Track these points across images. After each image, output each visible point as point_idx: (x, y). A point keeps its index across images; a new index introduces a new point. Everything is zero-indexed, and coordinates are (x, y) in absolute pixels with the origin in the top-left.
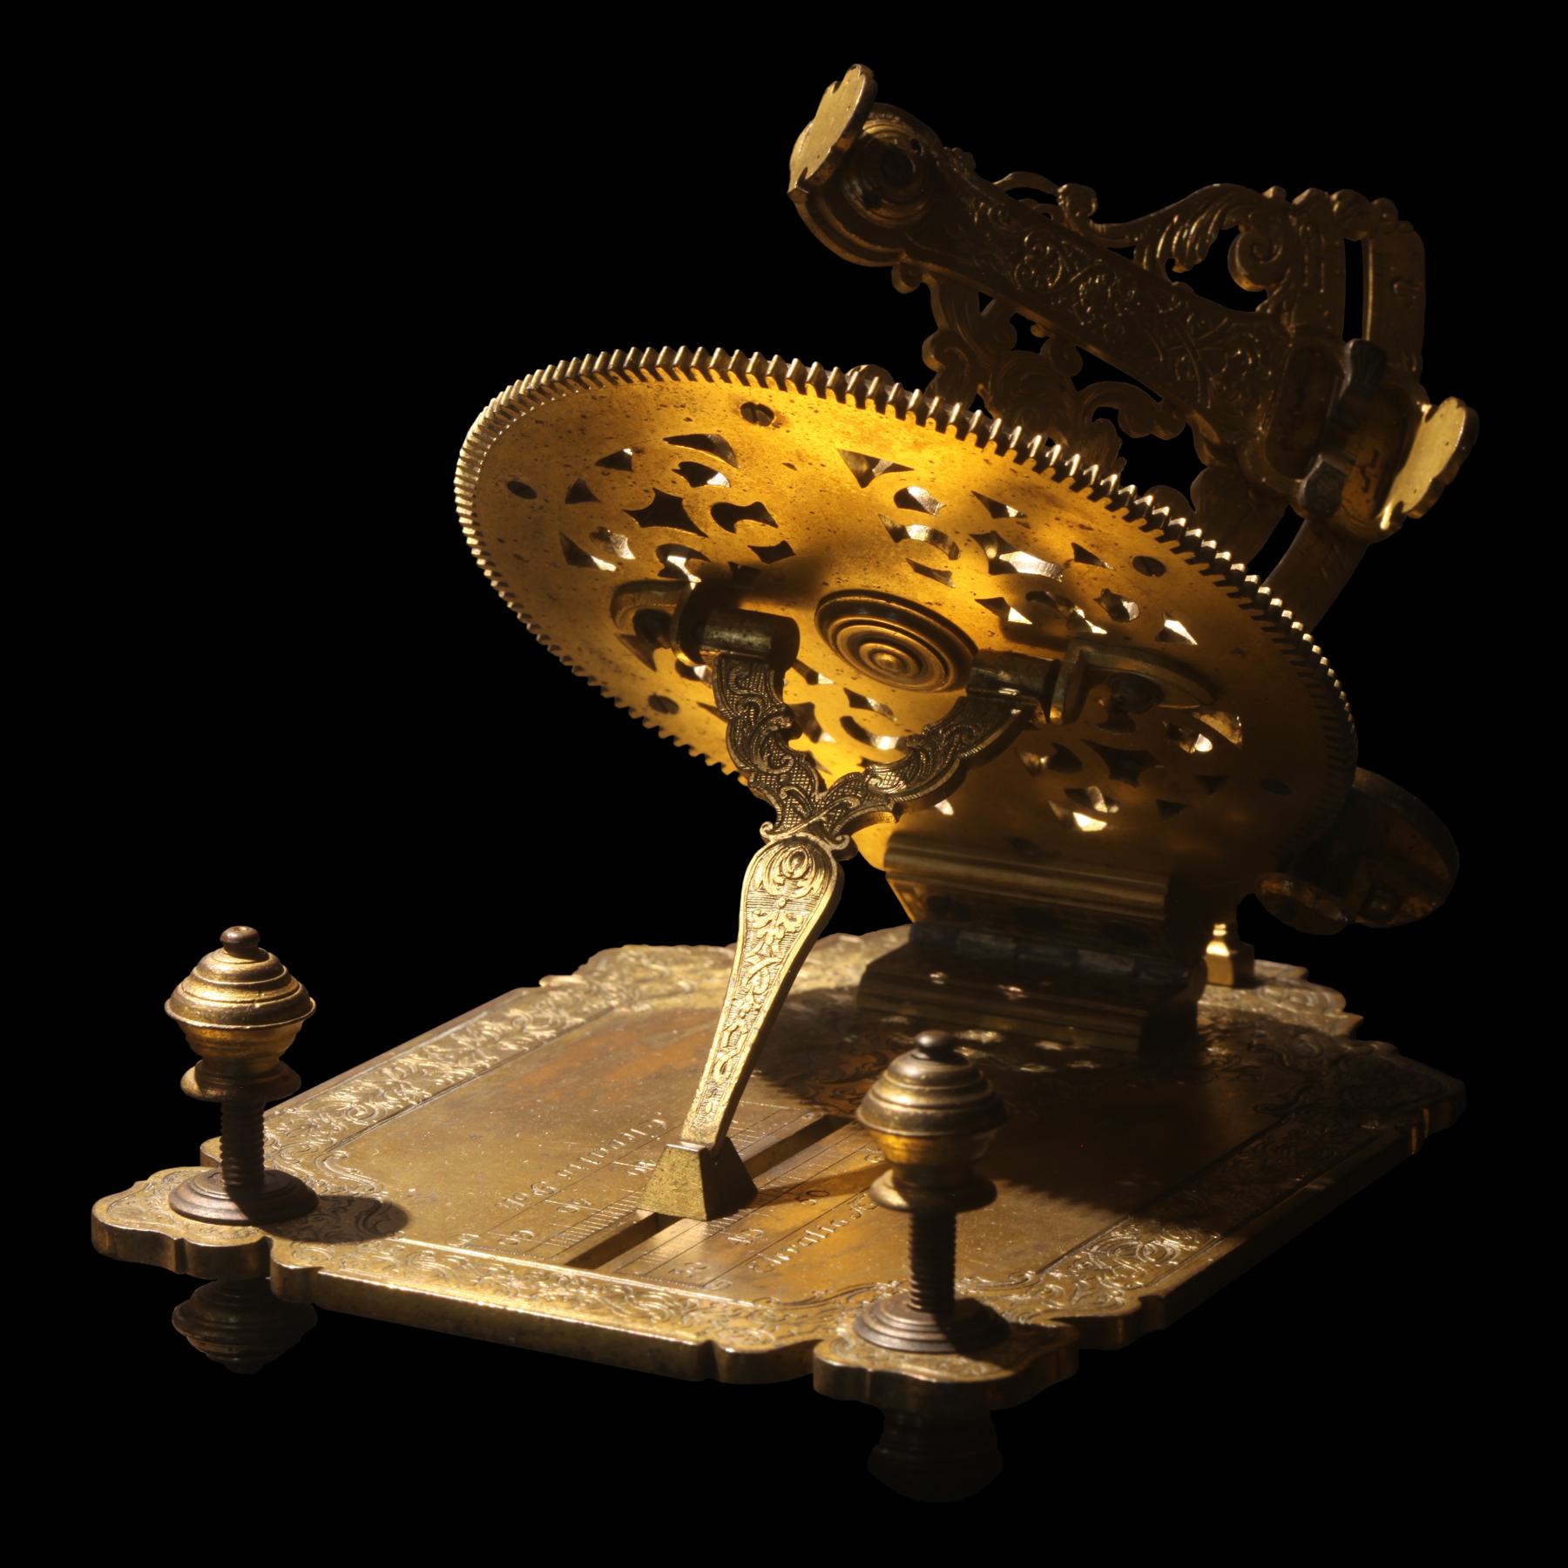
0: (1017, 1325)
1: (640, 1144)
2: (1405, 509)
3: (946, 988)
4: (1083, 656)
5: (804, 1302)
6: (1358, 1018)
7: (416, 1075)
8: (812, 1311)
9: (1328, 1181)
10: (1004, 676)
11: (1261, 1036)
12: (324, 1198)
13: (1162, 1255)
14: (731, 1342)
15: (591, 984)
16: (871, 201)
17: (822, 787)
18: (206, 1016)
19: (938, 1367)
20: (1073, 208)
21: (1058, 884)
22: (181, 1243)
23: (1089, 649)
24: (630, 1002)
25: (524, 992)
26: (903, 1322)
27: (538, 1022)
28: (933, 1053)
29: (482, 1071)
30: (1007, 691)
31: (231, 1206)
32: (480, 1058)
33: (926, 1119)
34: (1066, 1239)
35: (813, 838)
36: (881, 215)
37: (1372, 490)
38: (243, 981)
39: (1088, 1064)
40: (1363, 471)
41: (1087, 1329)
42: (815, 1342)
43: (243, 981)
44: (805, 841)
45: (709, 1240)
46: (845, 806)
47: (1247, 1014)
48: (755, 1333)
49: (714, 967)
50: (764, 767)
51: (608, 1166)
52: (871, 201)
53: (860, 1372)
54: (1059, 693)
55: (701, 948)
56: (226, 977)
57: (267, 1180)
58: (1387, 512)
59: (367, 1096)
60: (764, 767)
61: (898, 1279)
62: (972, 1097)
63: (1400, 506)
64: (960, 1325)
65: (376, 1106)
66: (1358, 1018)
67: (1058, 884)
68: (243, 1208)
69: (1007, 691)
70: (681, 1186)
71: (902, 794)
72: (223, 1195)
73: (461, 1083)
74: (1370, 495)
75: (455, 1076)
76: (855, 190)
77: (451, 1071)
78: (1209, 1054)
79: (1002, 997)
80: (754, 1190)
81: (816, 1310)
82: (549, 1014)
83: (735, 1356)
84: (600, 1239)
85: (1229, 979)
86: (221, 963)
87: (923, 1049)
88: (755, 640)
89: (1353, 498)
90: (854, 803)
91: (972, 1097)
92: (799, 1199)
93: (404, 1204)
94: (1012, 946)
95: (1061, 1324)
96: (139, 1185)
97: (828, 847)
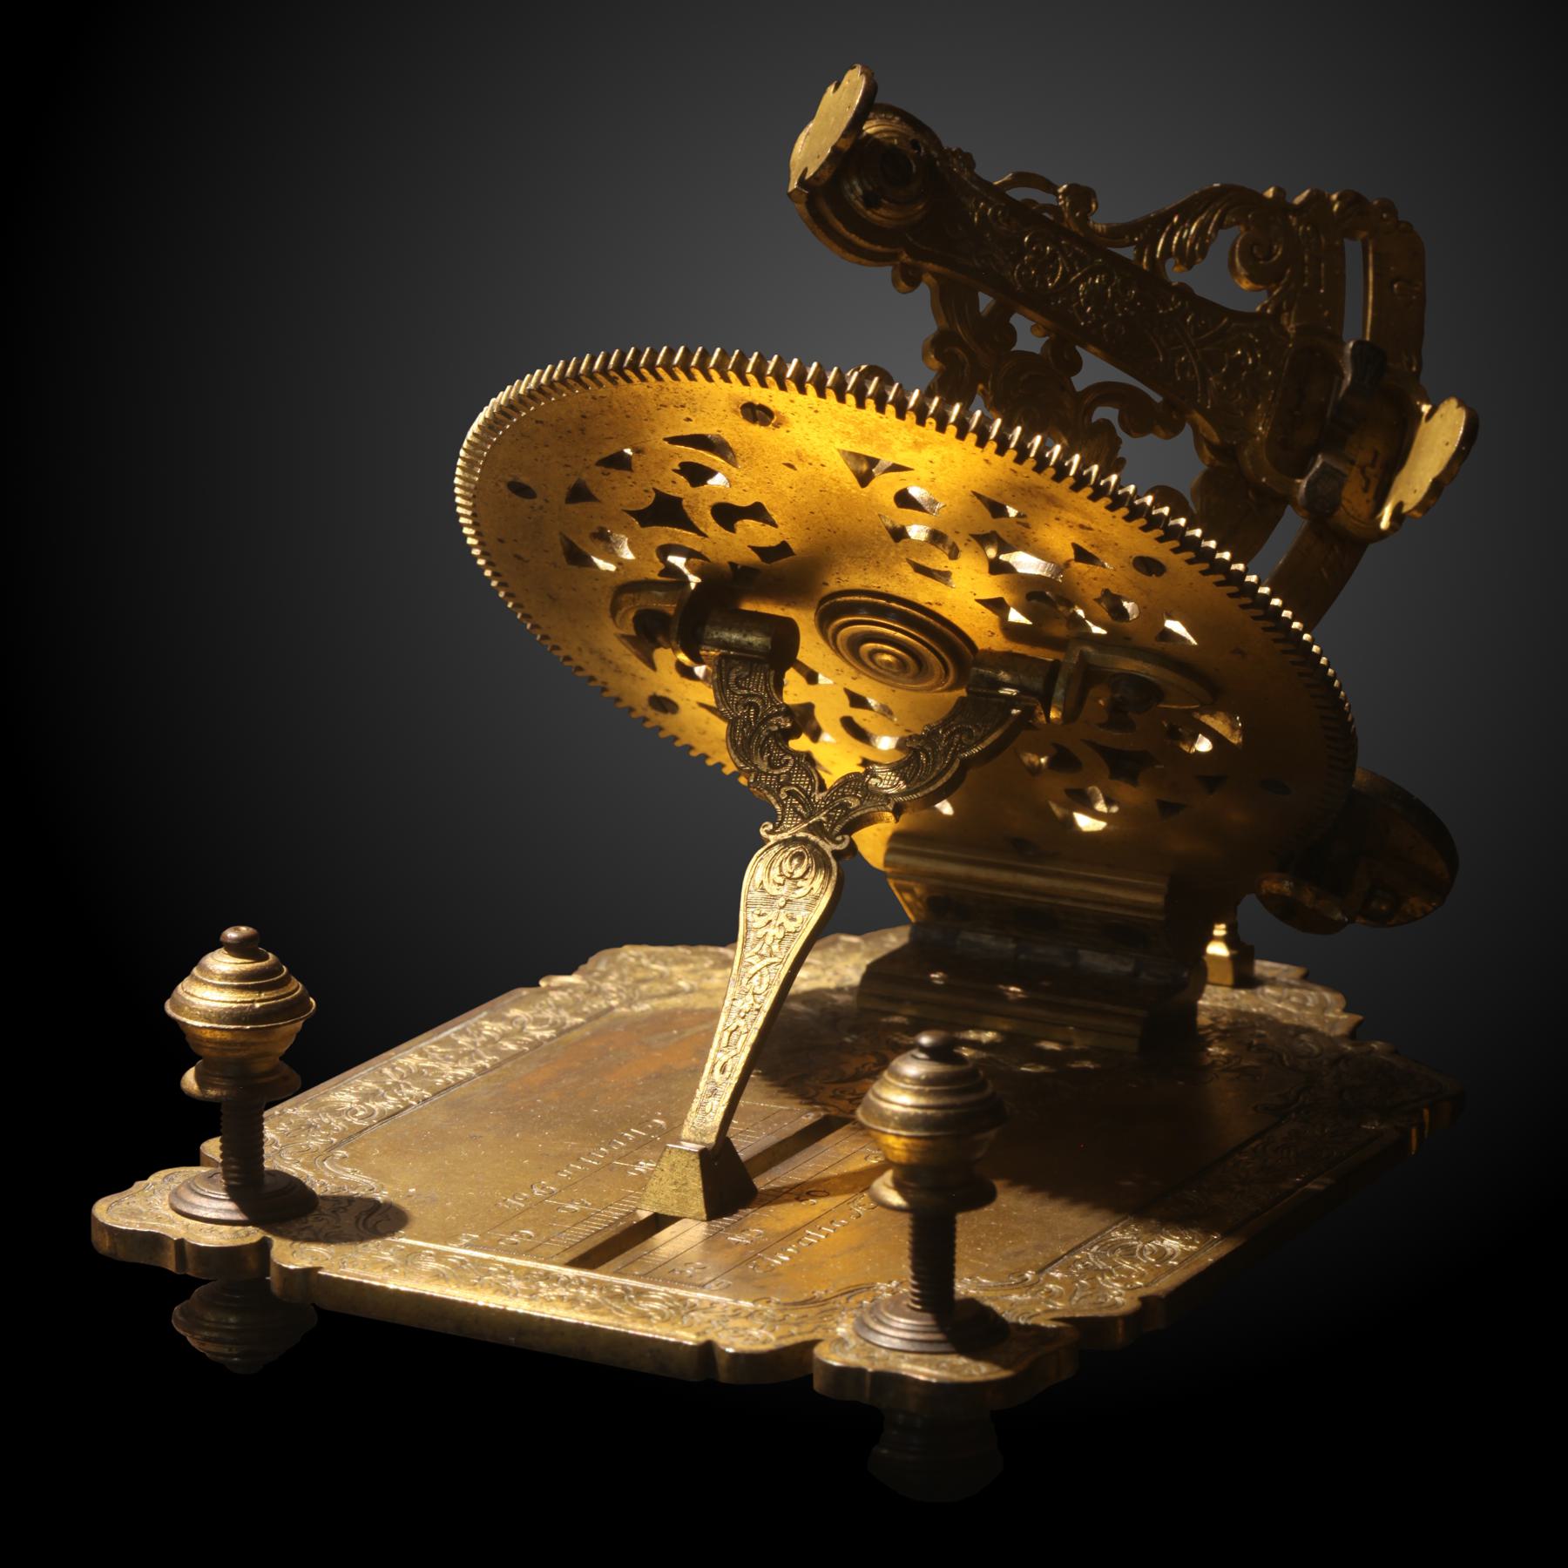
0: (1017, 1325)
1: (640, 1144)
2: (1405, 509)
3: (946, 988)
4: (1083, 656)
5: (804, 1302)
7: (416, 1075)
8: (812, 1311)
9: (1328, 1181)
10: (1004, 676)
11: (1261, 1036)
12: (324, 1198)
13: (1162, 1255)
14: (731, 1342)
15: (591, 984)
16: (871, 201)
17: (822, 787)
18: (206, 1016)
19: (938, 1367)
21: (1058, 884)
22: (181, 1243)
23: (1089, 649)
24: (630, 1002)
26: (903, 1322)
27: (538, 1022)
28: (933, 1053)
29: (482, 1071)
30: (1007, 691)
31: (231, 1206)
32: (480, 1058)
33: (926, 1119)
34: (1066, 1239)
35: (813, 838)
36: (881, 215)
37: (1372, 490)
38: (243, 981)
39: (1088, 1064)
40: (1363, 471)
42: (815, 1342)
43: (243, 981)
44: (805, 841)
45: (709, 1240)
46: (845, 806)
47: (1247, 1014)
48: (755, 1333)
49: (714, 967)
50: (764, 767)
51: (608, 1166)
52: (871, 201)
53: (860, 1372)
54: (1059, 693)
55: (701, 948)
56: (226, 977)
57: (267, 1180)
58: (1387, 512)
59: (367, 1096)
60: (764, 767)
61: (898, 1279)
62: (972, 1097)
63: (1400, 506)
64: (960, 1325)
65: (376, 1106)
67: (1058, 884)
68: (243, 1208)
69: (1007, 691)
70: (681, 1186)
71: (902, 794)
72: (223, 1195)
73: (461, 1083)
74: (1370, 495)
75: (455, 1076)
77: (451, 1071)
78: (1209, 1054)
79: (1002, 997)
80: (754, 1190)
81: (816, 1310)
82: (549, 1014)
83: (735, 1356)
85: (1229, 979)
86: (221, 963)
87: (923, 1049)
88: (755, 640)
89: (1353, 498)
90: (854, 803)
91: (972, 1097)
92: (799, 1199)
93: (404, 1204)
94: (1012, 946)
95: (1061, 1324)
96: (139, 1185)
97: (828, 847)
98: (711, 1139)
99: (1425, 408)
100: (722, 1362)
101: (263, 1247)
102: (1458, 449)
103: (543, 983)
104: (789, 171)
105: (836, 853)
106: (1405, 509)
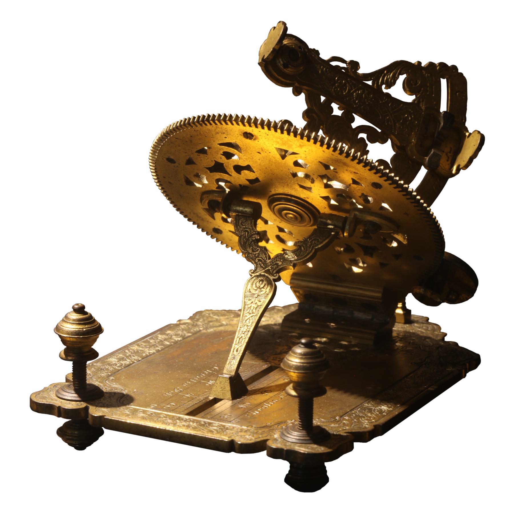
0: (333, 434)
1: (210, 375)
3: (310, 324)
4: (355, 215)
5: (264, 427)
8: (266, 430)
9: (435, 387)
10: (329, 222)
11: (413, 340)
12: (106, 393)
13: (381, 411)
15: (194, 323)
16: (285, 66)
17: (270, 258)
19: (307, 448)
21: (347, 290)
22: (59, 407)
23: (357, 213)
24: (206, 328)
26: (296, 433)
27: (176, 335)
28: (306, 345)
29: (158, 351)
30: (330, 227)
31: (76, 395)
32: (157, 347)
33: (304, 367)
34: (349, 406)
35: (266, 275)
37: (450, 161)
39: (357, 349)
40: (447, 154)
42: (267, 440)
44: (264, 276)
45: (233, 406)
46: (277, 264)
47: (409, 332)
48: (247, 437)
49: (234, 317)
50: (250, 251)
51: (199, 382)
52: (285, 66)
54: (347, 227)
56: (74, 320)
60: (250, 251)
62: (319, 360)
65: (123, 362)
67: (347, 290)
68: (80, 396)
69: (330, 227)
70: (223, 389)
71: (296, 260)
72: (73, 392)
73: (151, 355)
74: (449, 162)
75: (149, 353)
78: (396, 345)
79: (328, 327)
80: (247, 390)
81: (267, 429)
82: (180, 332)
83: (241, 445)
84: (197, 406)
85: (403, 321)
87: (303, 344)
88: (248, 210)
90: (280, 263)
91: (319, 360)
92: (262, 393)
93: (132, 395)
94: (332, 310)
95: (348, 434)
97: (271, 278)
98: (233, 373)
101: (86, 409)
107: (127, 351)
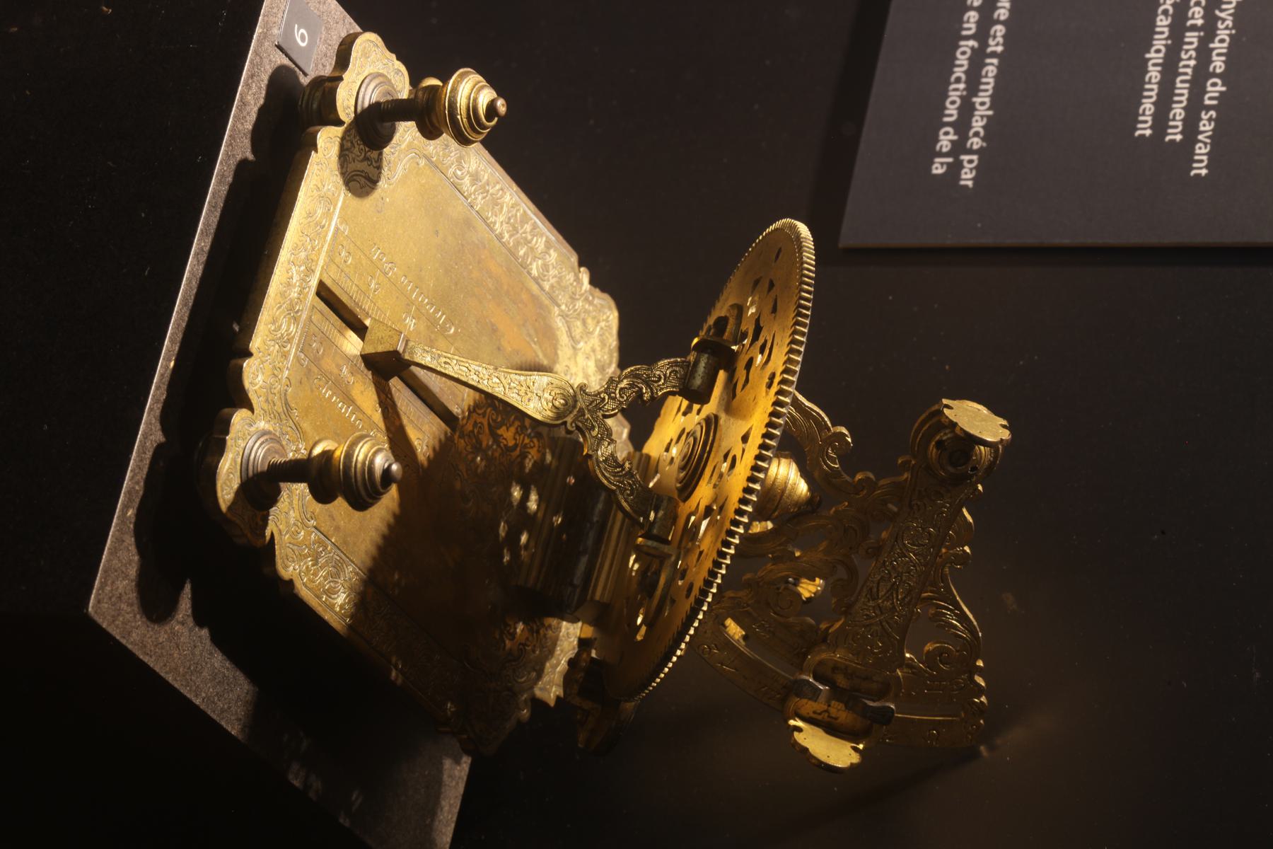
0: (268, 515)
1: (432, 322)
2: (796, 734)
3: (565, 484)
4: (670, 556)
5: (287, 403)
6: (552, 704)
7: (496, 203)
8: (279, 408)
9: (399, 681)
10: (661, 513)
11: (534, 651)
12: (381, 154)
13: (331, 592)
14: (249, 366)
15: (581, 295)
16: (940, 444)
17: (605, 417)
18: (454, 90)
19: (229, 473)
20: (956, 555)
21: (613, 543)
22: (341, 79)
23: (673, 558)
24: (564, 316)
25: (574, 259)
26: (261, 453)
27: (546, 267)
28: (387, 472)
29: (500, 237)
30: (652, 515)
31: (366, 105)
32: (511, 236)
33: (350, 467)
34: (345, 543)
35: (575, 412)
36: (932, 450)
37: (814, 716)
38: (472, 110)
39: (506, 558)
40: (826, 711)
41: (269, 549)
42: (251, 408)
43: (472, 110)
44: (574, 407)
45: (348, 359)
46: (593, 428)
47: (555, 645)
48: (260, 378)
49: (597, 361)
50: (622, 385)
51: (410, 303)
52: (940, 444)
53: (227, 433)
54: (650, 543)
55: (616, 355)
56: (475, 100)
57: (388, 124)
58: (799, 723)
59: (475, 178)
60: (622, 385)
61: (295, 451)
62: (363, 493)
63: (799, 730)
64: (262, 487)
65: (467, 181)
66: (552, 704)
67: (613, 543)
68: (364, 111)
69: (652, 515)
70: (380, 341)
71: (597, 459)
72: (374, 100)
73: (488, 225)
74: (812, 715)
75: (495, 223)
76: (945, 436)
77: (499, 222)
78: (516, 623)
79: (556, 513)
80: (388, 378)
81: (280, 410)
82: (552, 272)
83: (241, 367)
84: (344, 299)
85: (583, 636)
86: (486, 96)
87: (390, 466)
88: (698, 381)
89: (809, 707)
90: (594, 433)
91: (363, 493)
92: (381, 404)
93: (377, 194)
94: (595, 519)
95: (268, 538)
96: (394, 56)
97: (569, 419)
98: (407, 357)
99: (861, 746)
100: (239, 361)
101: (339, 123)
102: (821, 762)
103: (582, 269)
104: (954, 399)
105: (565, 423)
106: (796, 734)
107: (498, 187)
